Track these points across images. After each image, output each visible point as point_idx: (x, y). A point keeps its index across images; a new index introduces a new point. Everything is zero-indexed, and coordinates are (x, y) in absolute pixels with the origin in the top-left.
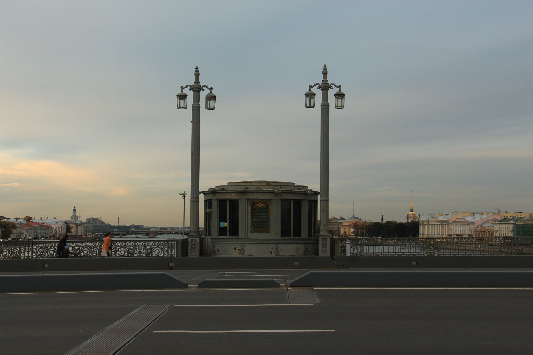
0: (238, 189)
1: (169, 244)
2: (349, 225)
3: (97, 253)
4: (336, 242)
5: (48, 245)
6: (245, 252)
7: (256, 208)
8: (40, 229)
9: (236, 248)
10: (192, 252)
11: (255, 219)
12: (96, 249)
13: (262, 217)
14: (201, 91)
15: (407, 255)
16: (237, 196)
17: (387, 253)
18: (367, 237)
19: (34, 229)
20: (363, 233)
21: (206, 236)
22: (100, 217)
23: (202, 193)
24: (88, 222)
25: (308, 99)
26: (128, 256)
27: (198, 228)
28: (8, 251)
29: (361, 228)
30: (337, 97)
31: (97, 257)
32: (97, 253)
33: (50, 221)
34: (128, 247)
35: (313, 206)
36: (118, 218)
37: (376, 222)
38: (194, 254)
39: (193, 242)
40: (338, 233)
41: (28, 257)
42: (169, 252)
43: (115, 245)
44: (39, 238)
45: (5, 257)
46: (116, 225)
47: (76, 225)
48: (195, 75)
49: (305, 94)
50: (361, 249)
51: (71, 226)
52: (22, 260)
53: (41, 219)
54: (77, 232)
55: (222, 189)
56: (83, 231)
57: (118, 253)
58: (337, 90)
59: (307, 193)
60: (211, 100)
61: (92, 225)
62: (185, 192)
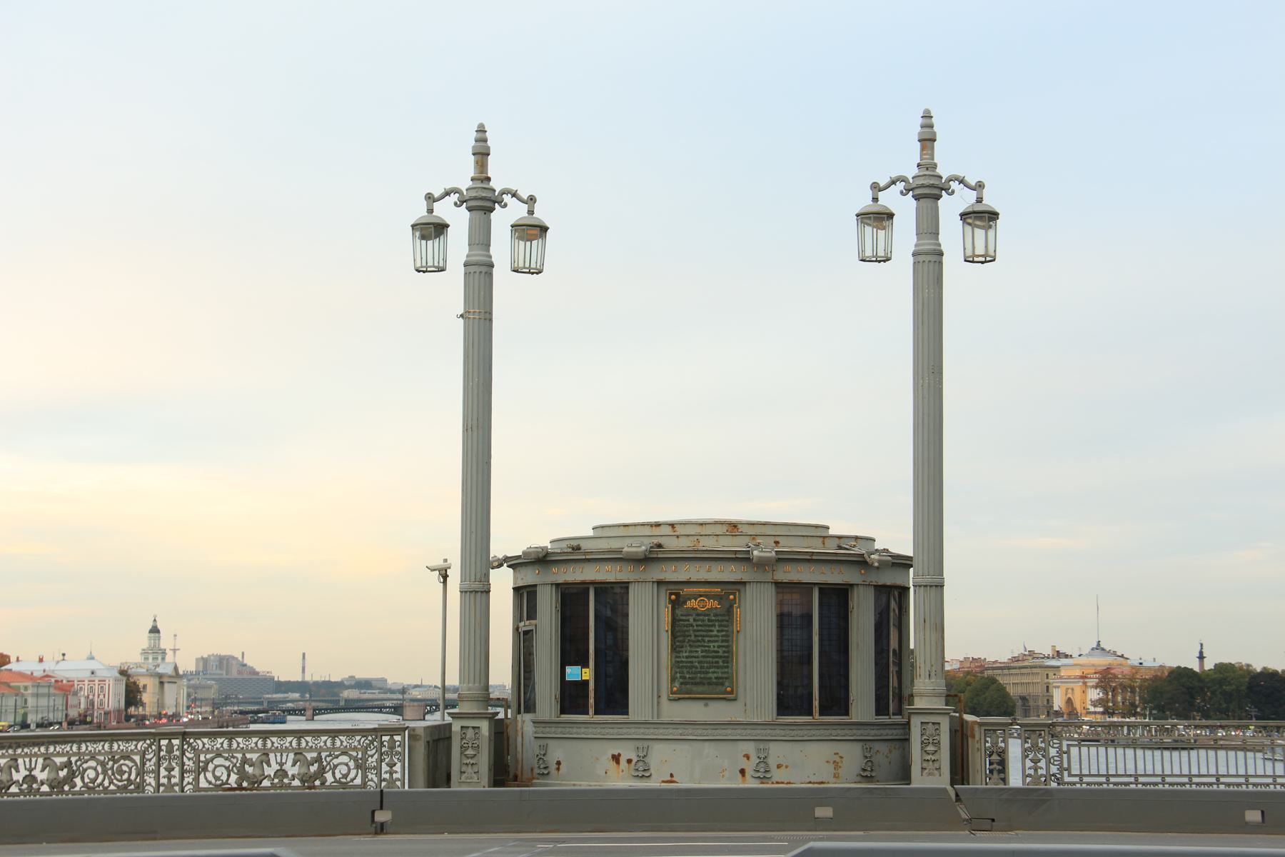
0: (626, 549)
1: (382, 743)
2: (1082, 677)
3: (133, 777)
4: (973, 736)
5: (55, 748)
6: (652, 771)
7: (689, 615)
8: (37, 695)
9: (619, 755)
10: (925, 769)
11: (685, 655)
12: (127, 762)
13: (711, 644)
14: (941, 196)
15: (1233, 784)
16: (621, 571)
17: (1103, 776)
18: (1145, 719)
19: (17, 695)
20: (1133, 705)
21: (519, 712)
22: (243, 653)
23: (505, 565)
24: (201, 669)
25: (868, 230)
26: (240, 788)
27: (487, 687)
28: (101, 765)
29: (1124, 687)
30: (970, 221)
31: (131, 791)
32: (133, 777)
33: (72, 668)
34: (239, 756)
35: (893, 605)
36: (304, 654)
37: (1179, 667)
38: (471, 778)
39: (468, 736)
40: (1045, 703)
41: (170, 786)
42: (161, 775)
43: (194, 749)
44: (33, 726)
45: (89, 788)
46: (297, 677)
47: (157, 681)
48: (474, 154)
49: (858, 215)
50: (1062, 761)
51: (141, 685)
52: (150, 798)
53: (41, 660)
54: (160, 703)
55: (573, 549)
56: (183, 701)
57: (206, 778)
58: (973, 195)
59: (868, 560)
60: (530, 239)
61: (213, 679)
62: (446, 560)
